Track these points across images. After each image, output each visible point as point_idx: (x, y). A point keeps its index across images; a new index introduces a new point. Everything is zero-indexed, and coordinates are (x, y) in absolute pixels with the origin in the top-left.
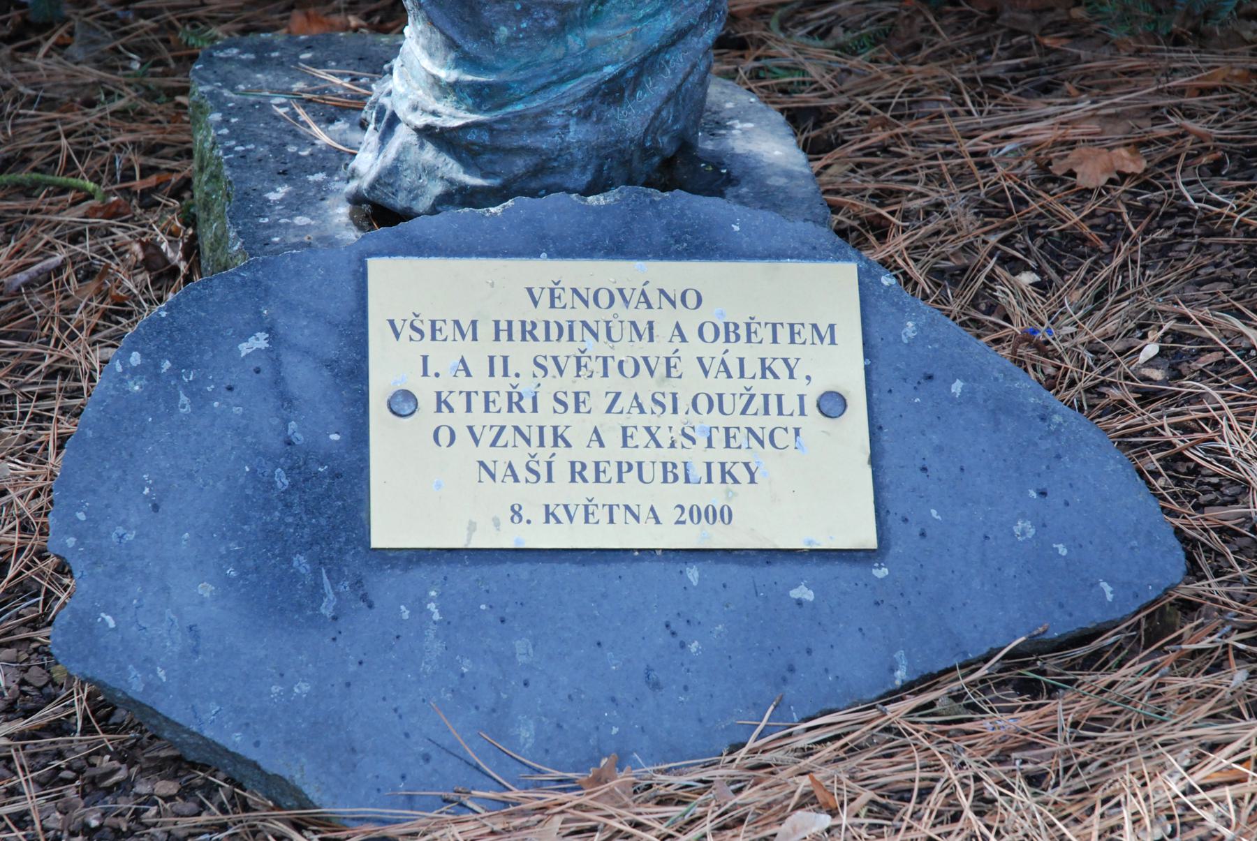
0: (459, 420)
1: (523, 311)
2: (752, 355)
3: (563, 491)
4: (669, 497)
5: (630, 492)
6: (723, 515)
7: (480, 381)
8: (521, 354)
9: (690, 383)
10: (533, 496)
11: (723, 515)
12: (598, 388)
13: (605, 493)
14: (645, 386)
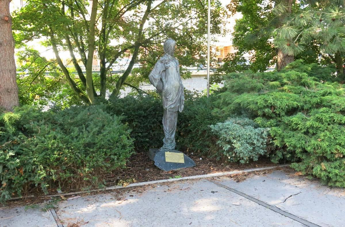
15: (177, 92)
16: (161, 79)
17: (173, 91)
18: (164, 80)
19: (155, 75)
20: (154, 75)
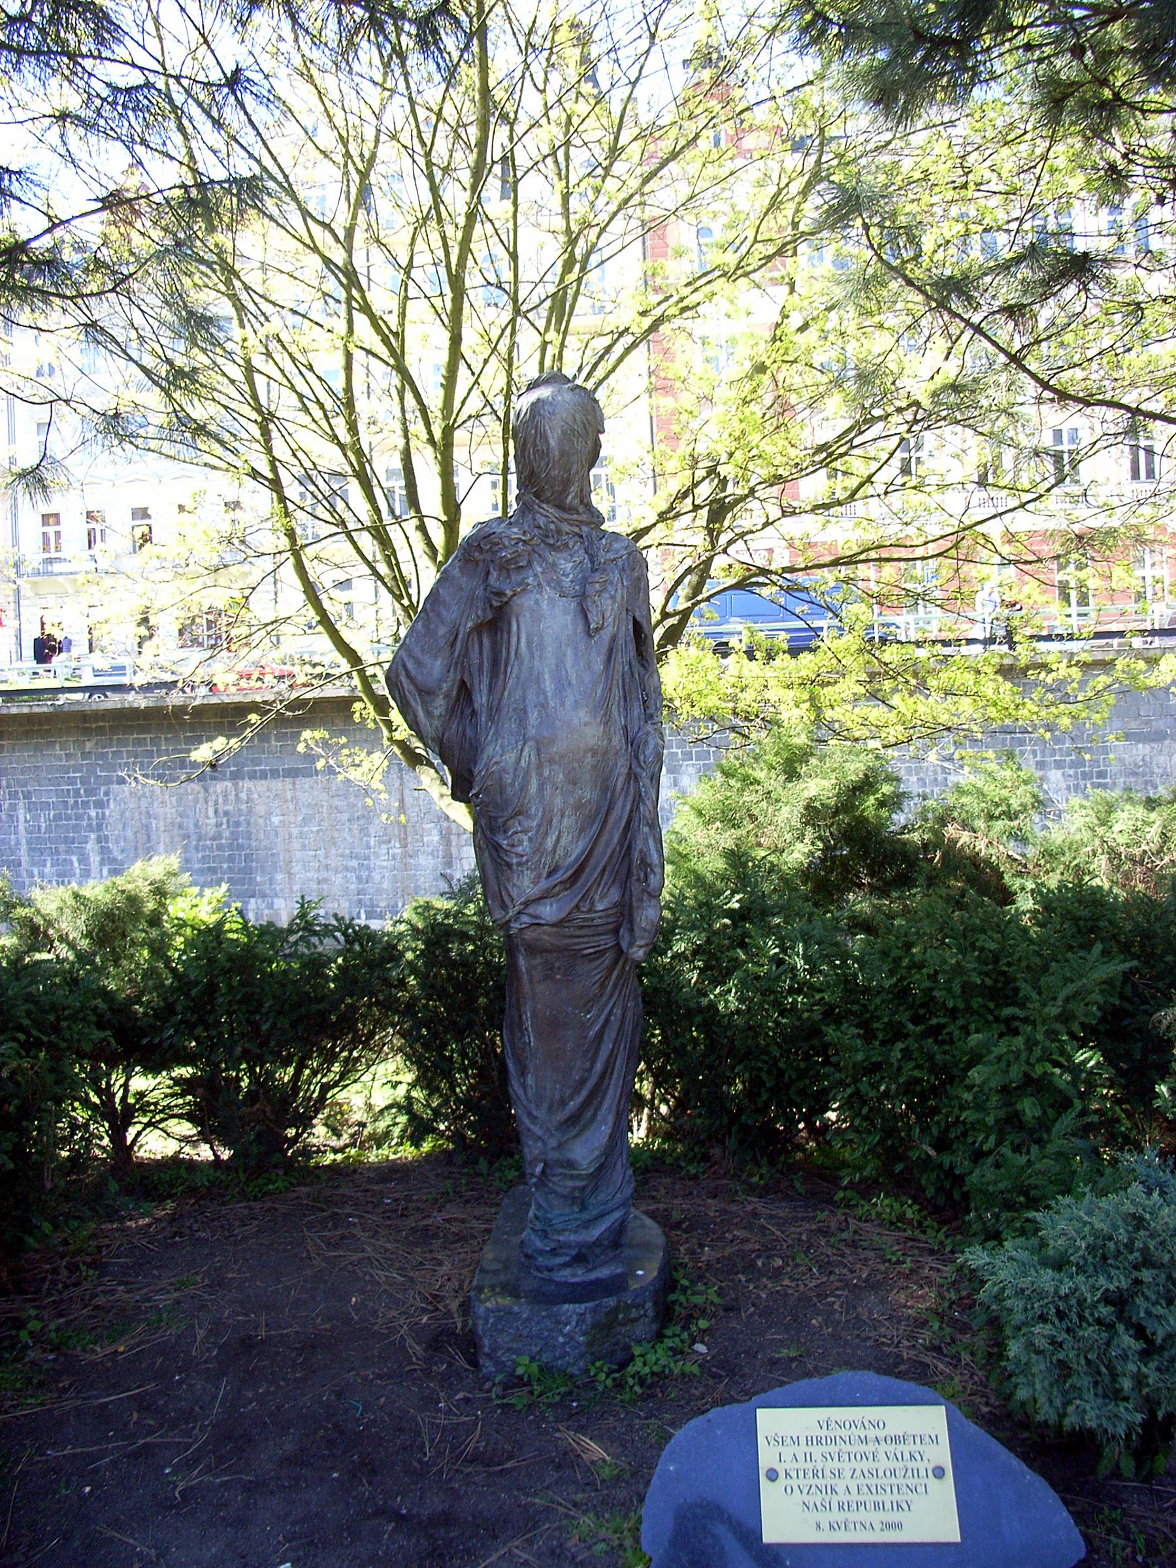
0: (794, 1483)
1: (816, 1432)
2: (906, 1449)
3: (836, 1516)
4: (876, 1518)
5: (861, 1516)
6: (899, 1526)
7: (802, 1465)
8: (817, 1451)
9: (883, 1464)
10: (825, 1518)
11: (899, 1526)
12: (847, 1467)
13: (852, 1516)
14: (866, 1465)
15: (588, 794)
16: (465, 692)
17: (541, 788)
18: (481, 699)
19: (427, 659)
20: (418, 663)
